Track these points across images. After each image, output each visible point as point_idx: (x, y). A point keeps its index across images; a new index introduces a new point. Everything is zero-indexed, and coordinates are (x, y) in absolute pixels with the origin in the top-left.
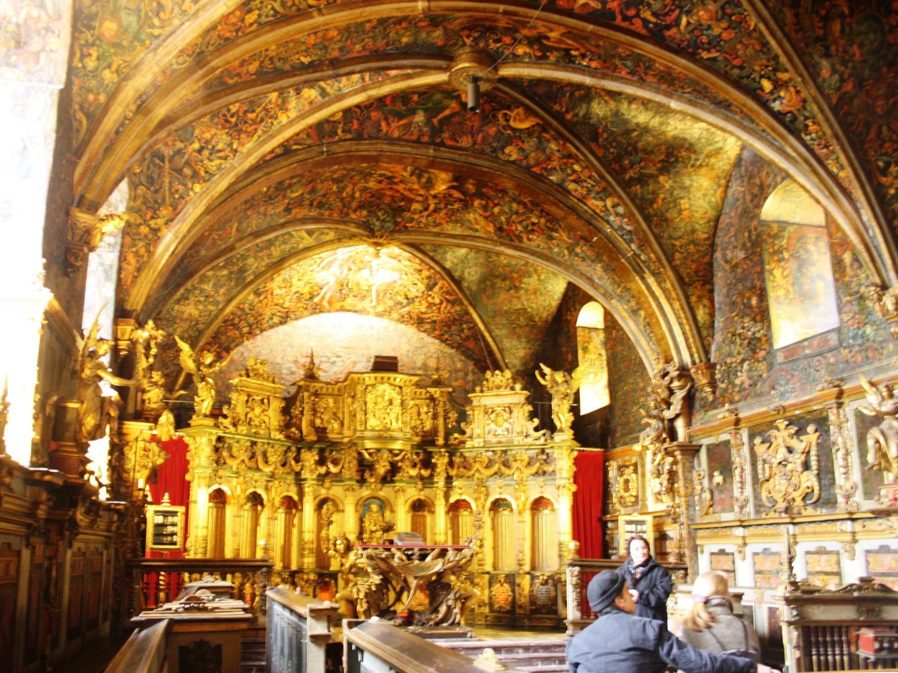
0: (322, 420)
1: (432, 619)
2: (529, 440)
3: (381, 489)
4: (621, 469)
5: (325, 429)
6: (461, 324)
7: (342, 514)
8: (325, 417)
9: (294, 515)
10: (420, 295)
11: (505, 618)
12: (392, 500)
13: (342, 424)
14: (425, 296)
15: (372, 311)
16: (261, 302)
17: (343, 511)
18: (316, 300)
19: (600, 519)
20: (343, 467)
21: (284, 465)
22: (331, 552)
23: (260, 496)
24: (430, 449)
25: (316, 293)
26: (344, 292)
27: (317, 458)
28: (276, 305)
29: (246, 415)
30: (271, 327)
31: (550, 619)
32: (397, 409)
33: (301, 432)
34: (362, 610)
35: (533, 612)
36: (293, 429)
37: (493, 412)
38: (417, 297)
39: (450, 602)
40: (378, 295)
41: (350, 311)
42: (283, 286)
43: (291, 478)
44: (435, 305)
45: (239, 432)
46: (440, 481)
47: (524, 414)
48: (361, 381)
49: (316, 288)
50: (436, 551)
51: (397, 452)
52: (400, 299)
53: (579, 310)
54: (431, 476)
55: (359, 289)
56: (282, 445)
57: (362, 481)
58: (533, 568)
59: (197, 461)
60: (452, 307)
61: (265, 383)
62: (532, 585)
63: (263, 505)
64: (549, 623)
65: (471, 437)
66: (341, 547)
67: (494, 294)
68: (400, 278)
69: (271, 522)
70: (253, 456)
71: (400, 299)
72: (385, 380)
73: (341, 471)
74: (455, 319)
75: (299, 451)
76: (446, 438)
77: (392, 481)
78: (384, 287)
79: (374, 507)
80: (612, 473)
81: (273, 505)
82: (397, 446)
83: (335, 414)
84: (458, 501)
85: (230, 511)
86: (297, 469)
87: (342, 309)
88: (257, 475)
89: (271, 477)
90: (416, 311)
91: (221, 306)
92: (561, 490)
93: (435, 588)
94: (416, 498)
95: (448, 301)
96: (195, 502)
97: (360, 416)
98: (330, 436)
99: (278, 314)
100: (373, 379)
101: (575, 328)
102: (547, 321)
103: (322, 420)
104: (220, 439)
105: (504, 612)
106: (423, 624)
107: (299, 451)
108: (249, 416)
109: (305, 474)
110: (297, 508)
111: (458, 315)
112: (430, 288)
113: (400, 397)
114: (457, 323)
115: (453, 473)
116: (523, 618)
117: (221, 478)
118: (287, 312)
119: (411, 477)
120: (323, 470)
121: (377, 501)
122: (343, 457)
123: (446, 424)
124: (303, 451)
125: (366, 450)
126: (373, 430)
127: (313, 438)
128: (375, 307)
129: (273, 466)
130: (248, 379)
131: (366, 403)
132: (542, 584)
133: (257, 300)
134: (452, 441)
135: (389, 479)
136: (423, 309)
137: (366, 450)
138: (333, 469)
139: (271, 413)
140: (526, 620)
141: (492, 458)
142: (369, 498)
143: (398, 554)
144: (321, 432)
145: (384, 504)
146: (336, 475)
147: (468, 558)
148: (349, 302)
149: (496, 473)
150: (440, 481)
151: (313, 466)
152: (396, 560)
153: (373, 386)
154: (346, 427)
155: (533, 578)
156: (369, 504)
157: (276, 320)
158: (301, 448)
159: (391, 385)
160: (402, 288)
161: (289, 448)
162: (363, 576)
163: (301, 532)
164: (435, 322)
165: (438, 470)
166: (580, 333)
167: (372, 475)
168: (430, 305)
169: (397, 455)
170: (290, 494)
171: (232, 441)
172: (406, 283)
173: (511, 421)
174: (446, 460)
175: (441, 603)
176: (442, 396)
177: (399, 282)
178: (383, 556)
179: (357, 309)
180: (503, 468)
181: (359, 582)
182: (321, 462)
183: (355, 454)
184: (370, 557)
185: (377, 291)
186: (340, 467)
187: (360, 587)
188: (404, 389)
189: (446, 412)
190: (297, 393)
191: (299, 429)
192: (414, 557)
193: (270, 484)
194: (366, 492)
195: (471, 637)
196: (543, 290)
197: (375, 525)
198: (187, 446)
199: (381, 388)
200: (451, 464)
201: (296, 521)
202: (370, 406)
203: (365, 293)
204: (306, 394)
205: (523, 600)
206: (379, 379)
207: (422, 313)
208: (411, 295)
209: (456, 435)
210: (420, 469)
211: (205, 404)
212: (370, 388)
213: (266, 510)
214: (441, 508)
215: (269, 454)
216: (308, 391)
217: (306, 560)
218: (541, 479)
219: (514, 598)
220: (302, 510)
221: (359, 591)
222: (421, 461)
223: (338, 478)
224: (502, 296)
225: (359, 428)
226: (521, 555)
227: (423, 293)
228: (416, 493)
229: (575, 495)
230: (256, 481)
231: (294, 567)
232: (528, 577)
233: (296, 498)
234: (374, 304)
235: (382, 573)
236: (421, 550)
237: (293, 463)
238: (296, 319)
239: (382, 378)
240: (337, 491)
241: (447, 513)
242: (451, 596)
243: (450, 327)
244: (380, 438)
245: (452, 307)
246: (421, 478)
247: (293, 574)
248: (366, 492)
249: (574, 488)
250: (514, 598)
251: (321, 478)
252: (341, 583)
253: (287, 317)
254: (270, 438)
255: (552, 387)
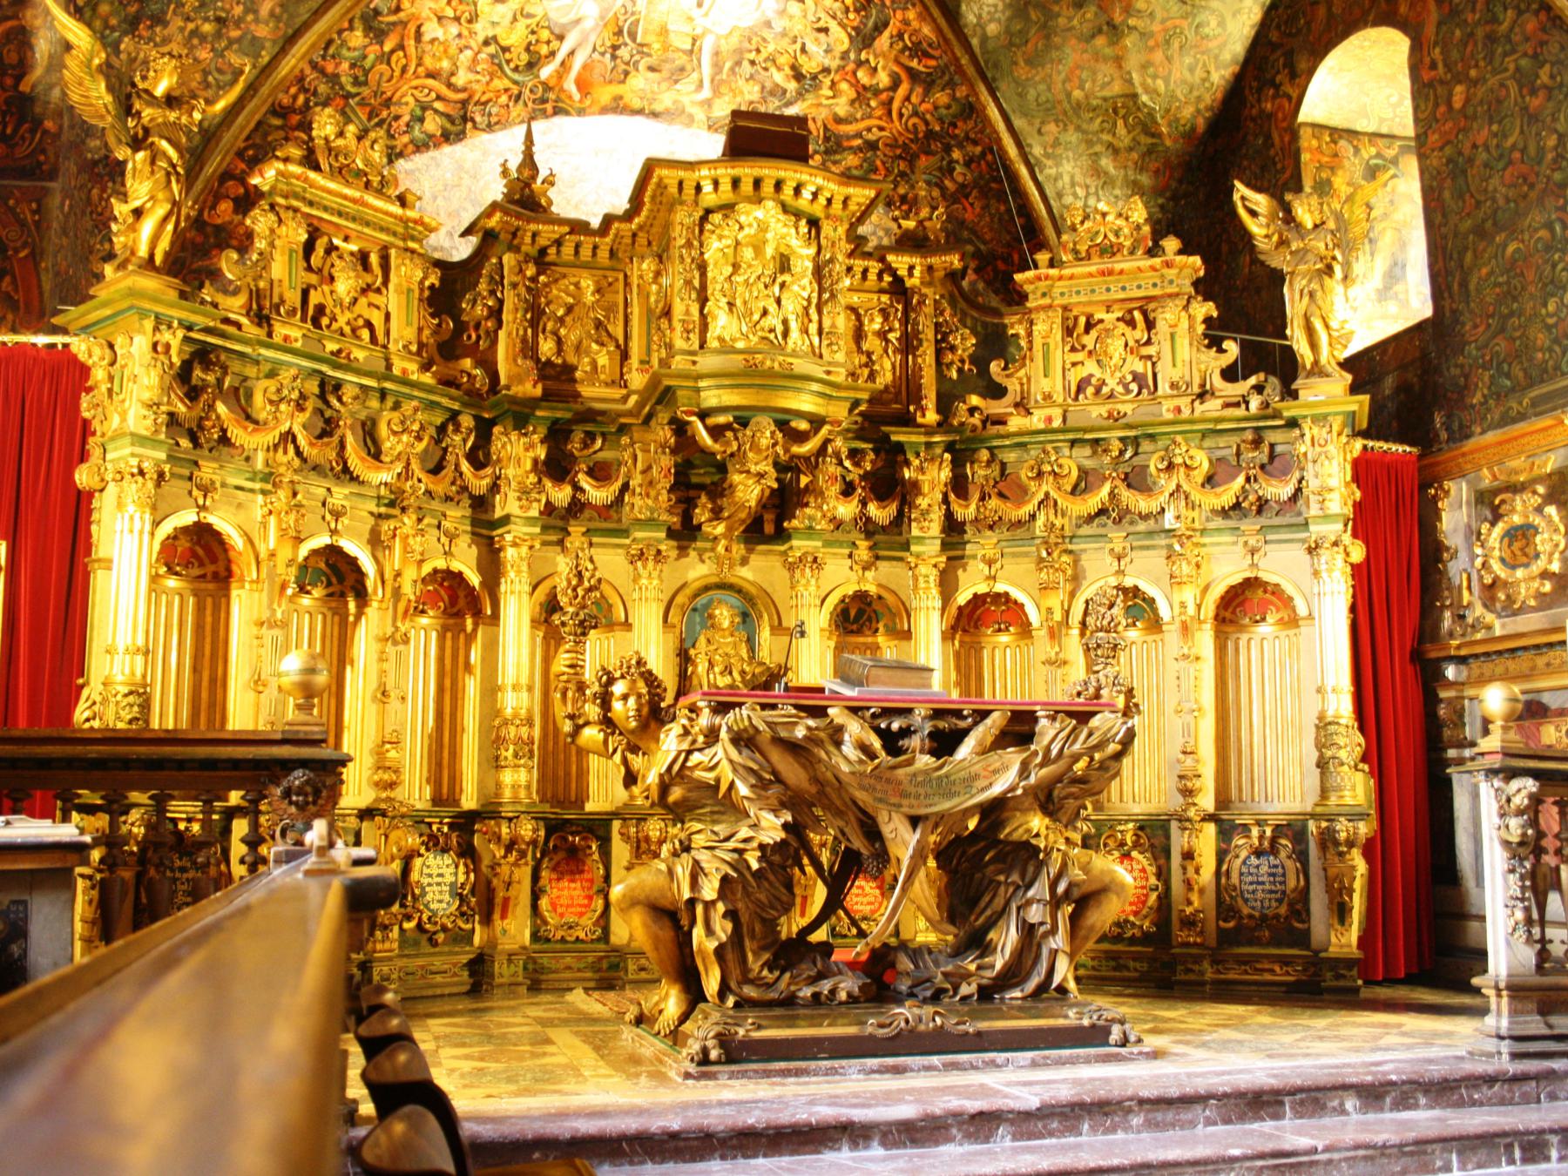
0: (559, 342)
1: (967, 976)
2: (1212, 406)
3: (744, 561)
4: (1490, 504)
5: (568, 370)
6: (948, 149)
7: (619, 634)
8: (571, 335)
9: (470, 638)
10: (834, 64)
11: (1136, 957)
12: (780, 594)
13: (625, 356)
14: (851, 64)
15: (700, 114)
16: (386, 58)
17: (627, 625)
18: (546, 72)
19: (1417, 656)
20: (625, 487)
21: (436, 470)
22: (592, 734)
23: (353, 562)
24: (899, 436)
25: (544, 50)
26: (623, 53)
27: (542, 452)
28: (431, 75)
29: (305, 294)
30: (420, 147)
31: (1285, 961)
32: (802, 286)
33: (494, 376)
34: (711, 945)
35: (1225, 938)
36: (467, 363)
37: (1089, 327)
38: (826, 70)
39: (1035, 914)
40: (717, 67)
41: (640, 112)
42: (450, 13)
43: (457, 516)
44: (877, 92)
45: (277, 339)
46: (927, 532)
47: (1191, 328)
48: (689, 191)
49: (545, 35)
50: (995, 721)
51: (803, 425)
52: (780, 78)
53: (1311, 72)
54: (900, 521)
55: (666, 47)
56: (432, 405)
57: (685, 533)
58: (1223, 801)
59: (115, 421)
60: (927, 93)
61: (371, 199)
62: (1221, 856)
63: (362, 595)
64: (1280, 975)
65: (1022, 406)
66: (624, 710)
67: (1049, 47)
68: (782, 12)
69: (390, 649)
70: (327, 428)
71: (780, 78)
72: (767, 188)
73: (619, 500)
74: (930, 134)
75: (484, 430)
76: (945, 405)
77: (781, 535)
78: (734, 41)
79: (724, 616)
80: (1453, 519)
81: (397, 593)
82: (804, 402)
83: (599, 325)
84: (978, 600)
85: (244, 604)
86: (480, 484)
87: (618, 107)
88: (340, 494)
89: (392, 504)
90: (822, 114)
91: (265, 58)
92: (1325, 554)
93: (977, 863)
94: (850, 589)
95: (913, 75)
96: (108, 564)
97: (684, 307)
98: (586, 391)
99: (438, 105)
100: (726, 186)
101: (1293, 132)
102: (1189, 135)
103: (559, 342)
104: (202, 355)
105: (1133, 940)
106: (936, 997)
107: (484, 430)
108: (315, 298)
109: (508, 504)
110: (477, 613)
111: (941, 120)
112: (864, 39)
113: (812, 251)
114: (936, 146)
115: (966, 511)
116: (1198, 959)
117: (206, 490)
118: (464, 103)
119: (838, 524)
120: (561, 495)
121: (734, 599)
122: (627, 456)
123: (941, 376)
124: (497, 430)
125: (703, 415)
126: (726, 348)
127: (530, 388)
128: (708, 103)
129: (399, 467)
130: (312, 175)
131: (703, 268)
132: (1258, 853)
133: (373, 51)
134: (961, 415)
135: (769, 528)
136: (842, 108)
137: (703, 415)
138: (597, 494)
139: (393, 300)
140: (1206, 965)
141: (1089, 464)
142: (707, 588)
143: (855, 729)
144: (557, 378)
145: (750, 606)
146: (605, 511)
147: (1113, 748)
148: (639, 84)
149: (1102, 512)
150: (927, 532)
151: (533, 478)
152: (849, 749)
153: (728, 208)
154: (634, 361)
155: (1226, 831)
156: (707, 606)
157: (432, 124)
158: (493, 423)
159: (785, 209)
160: (784, 43)
161: (454, 416)
162: (715, 818)
163: (491, 690)
164: (872, 146)
165: (923, 502)
166: (1307, 141)
167: (717, 514)
168: (862, 94)
169: (801, 437)
170: (456, 566)
171: (251, 371)
172: (798, 27)
173: (1151, 350)
174: (946, 474)
175: (1003, 912)
176: (930, 284)
177: (778, 25)
178: (800, 732)
179: (658, 107)
180: (1127, 496)
181: (699, 840)
182: (557, 467)
183: (665, 434)
184: (744, 740)
185: (717, 54)
186: (617, 485)
187: (703, 857)
188: (827, 228)
189: (940, 330)
190: (479, 255)
191: (488, 364)
192: (915, 742)
193: (386, 526)
194: (697, 570)
195: (1124, 1042)
196: (1190, 34)
197: (728, 670)
198: (85, 371)
199: (750, 215)
200: (959, 486)
201: (475, 655)
202: (718, 273)
203: (682, 60)
204: (509, 259)
205: (1199, 903)
206: (747, 187)
207: (839, 120)
208: (809, 66)
209: (975, 400)
210: (864, 503)
211: (148, 226)
212: (716, 218)
213: (372, 611)
214: (929, 625)
215: (383, 430)
216: (516, 249)
217: (507, 777)
218: (1250, 525)
219: (1165, 898)
220: (495, 617)
221: (697, 872)
222: (865, 477)
223: (610, 523)
224: (1072, 54)
225: (679, 343)
226: (1189, 761)
227: (844, 56)
228: (853, 576)
229: (1360, 573)
230: (337, 515)
231: (469, 802)
232: (1211, 829)
233: (474, 579)
234: (707, 93)
235: (791, 801)
236: (938, 714)
237: (465, 466)
238: (490, 127)
239: (757, 183)
240: (610, 561)
241: (948, 636)
242: (1040, 889)
243: (911, 160)
244: (752, 374)
245: (927, 93)
246: (869, 528)
247: (466, 823)
248: (697, 570)
249: (1358, 553)
250: (1165, 898)
251: (556, 521)
252: (621, 851)
253: (465, 119)
254: (387, 374)
255: (1283, 243)
